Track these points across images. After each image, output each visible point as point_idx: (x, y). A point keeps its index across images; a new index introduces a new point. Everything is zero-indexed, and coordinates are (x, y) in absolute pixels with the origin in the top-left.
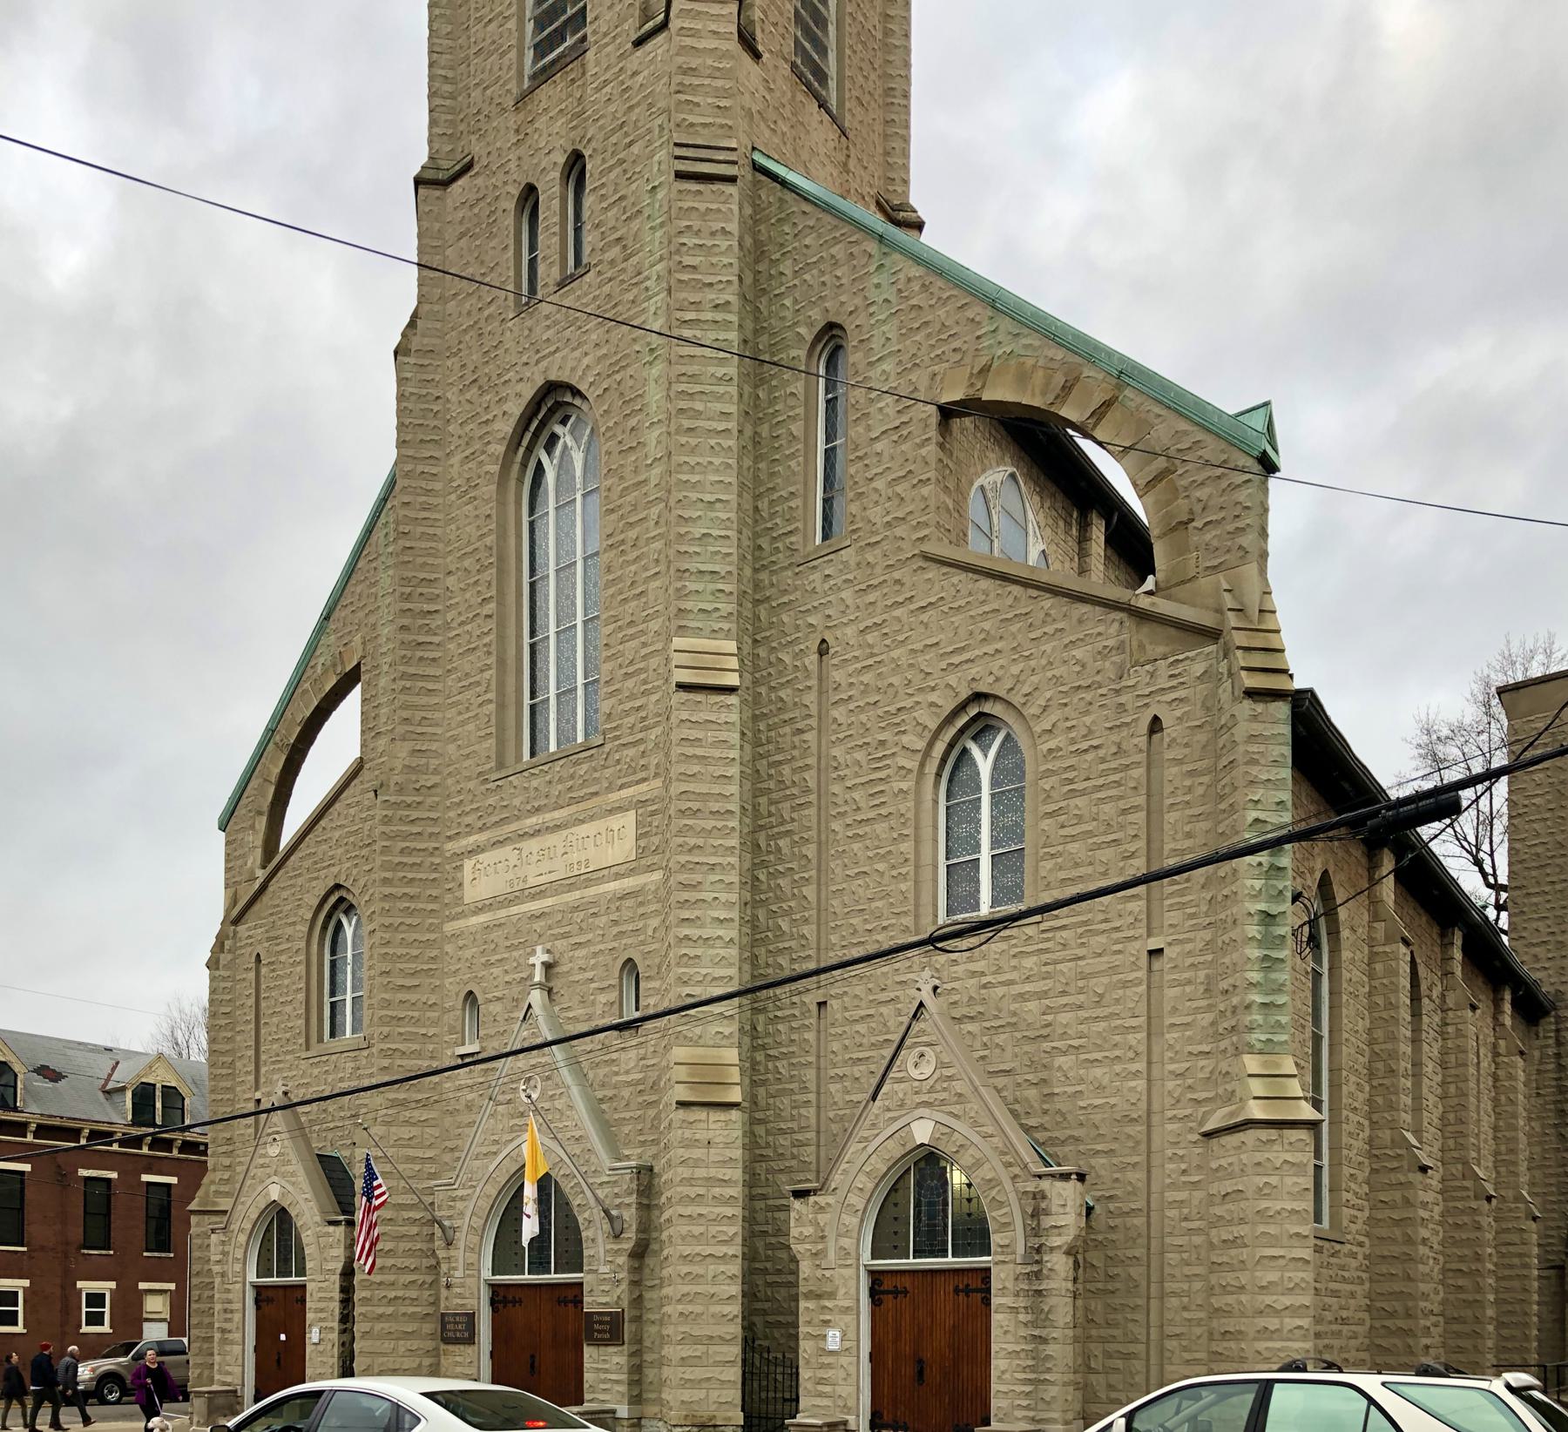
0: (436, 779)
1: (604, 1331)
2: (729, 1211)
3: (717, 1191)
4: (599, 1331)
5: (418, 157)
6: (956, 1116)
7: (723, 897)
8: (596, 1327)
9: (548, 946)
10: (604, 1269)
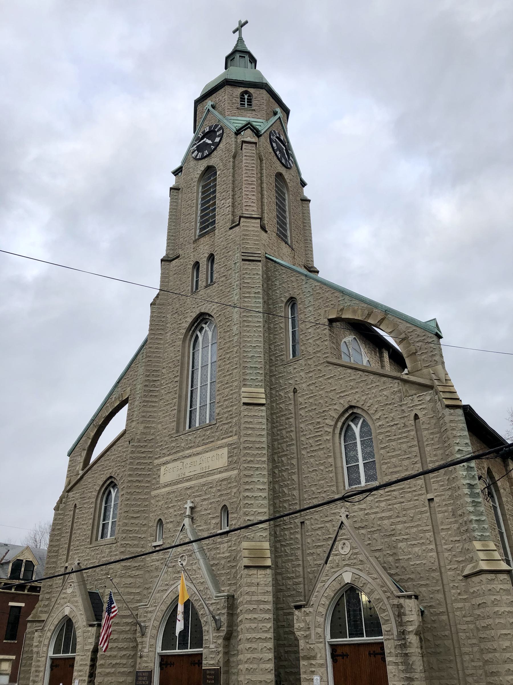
0: (153, 437)
1: (211, 679)
2: (267, 616)
3: (262, 607)
4: (209, 679)
5: (163, 254)
6: (361, 570)
7: (261, 480)
8: (208, 677)
9: (192, 500)
10: (212, 646)
